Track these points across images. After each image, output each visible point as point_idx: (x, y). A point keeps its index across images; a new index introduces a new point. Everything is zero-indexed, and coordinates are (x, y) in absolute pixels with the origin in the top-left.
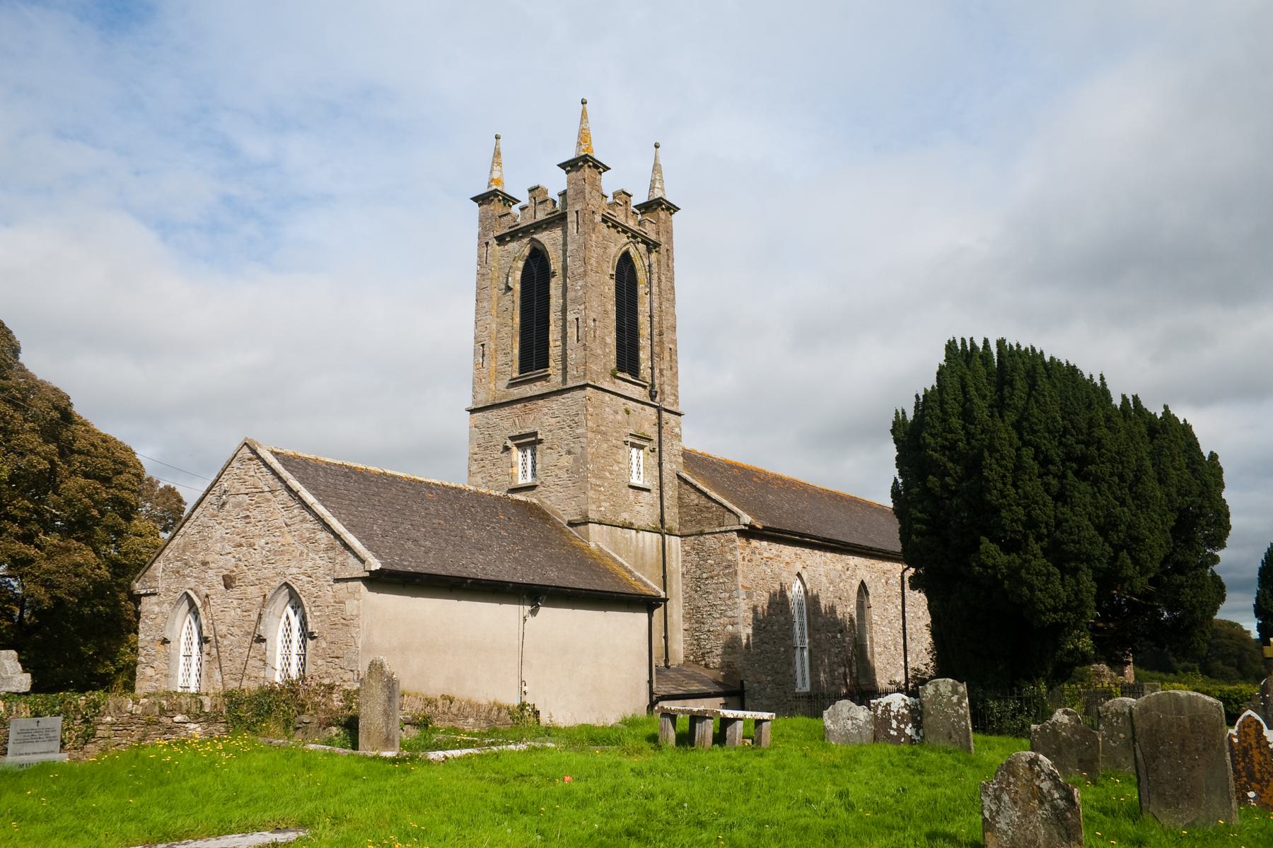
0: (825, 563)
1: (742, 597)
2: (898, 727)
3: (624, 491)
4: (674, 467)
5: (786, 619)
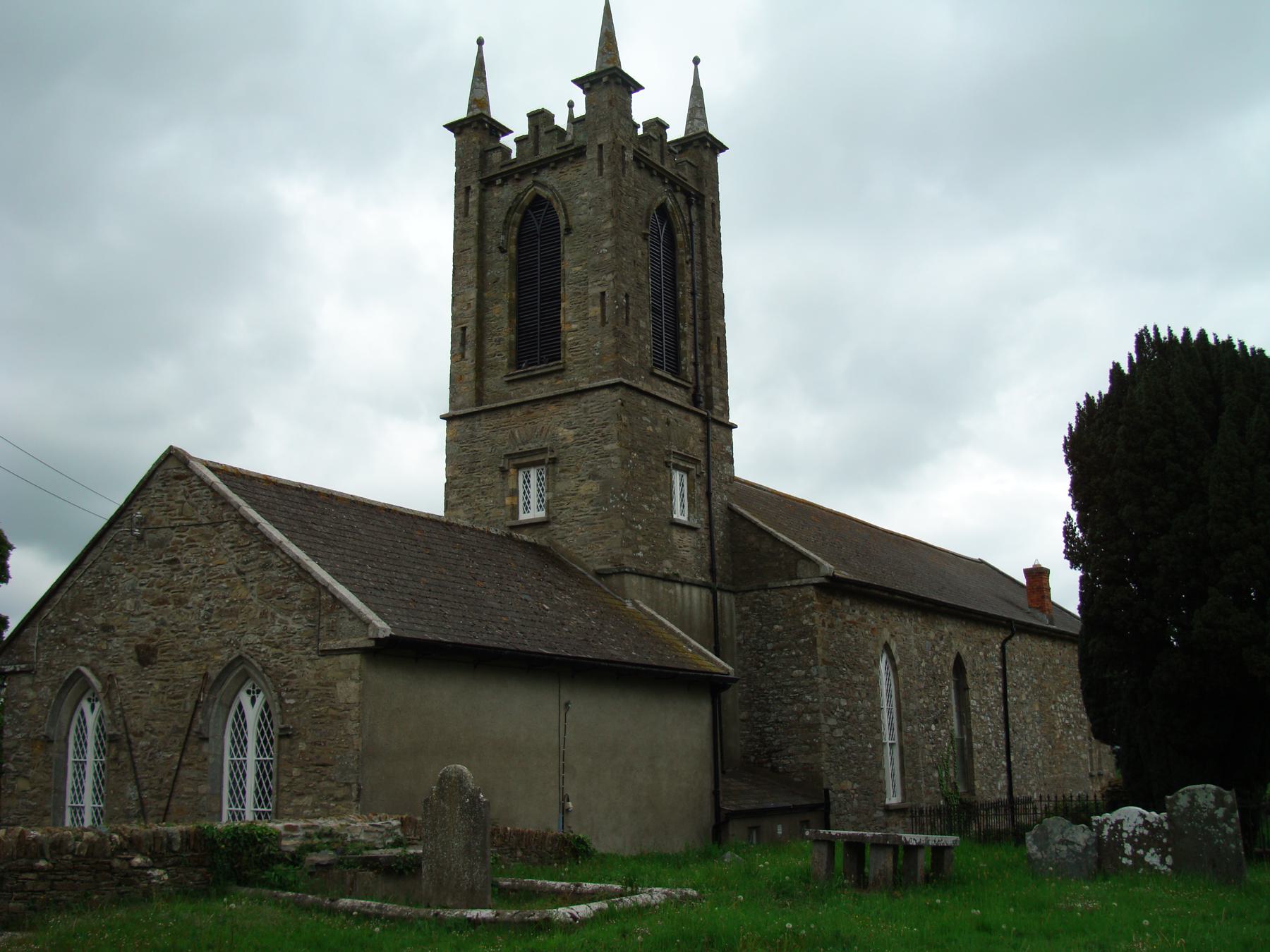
0: (916, 630)
1: (822, 676)
2: (1134, 853)
3: (665, 530)
4: (725, 498)
5: (873, 705)
